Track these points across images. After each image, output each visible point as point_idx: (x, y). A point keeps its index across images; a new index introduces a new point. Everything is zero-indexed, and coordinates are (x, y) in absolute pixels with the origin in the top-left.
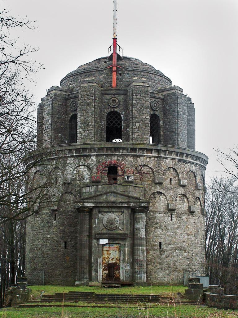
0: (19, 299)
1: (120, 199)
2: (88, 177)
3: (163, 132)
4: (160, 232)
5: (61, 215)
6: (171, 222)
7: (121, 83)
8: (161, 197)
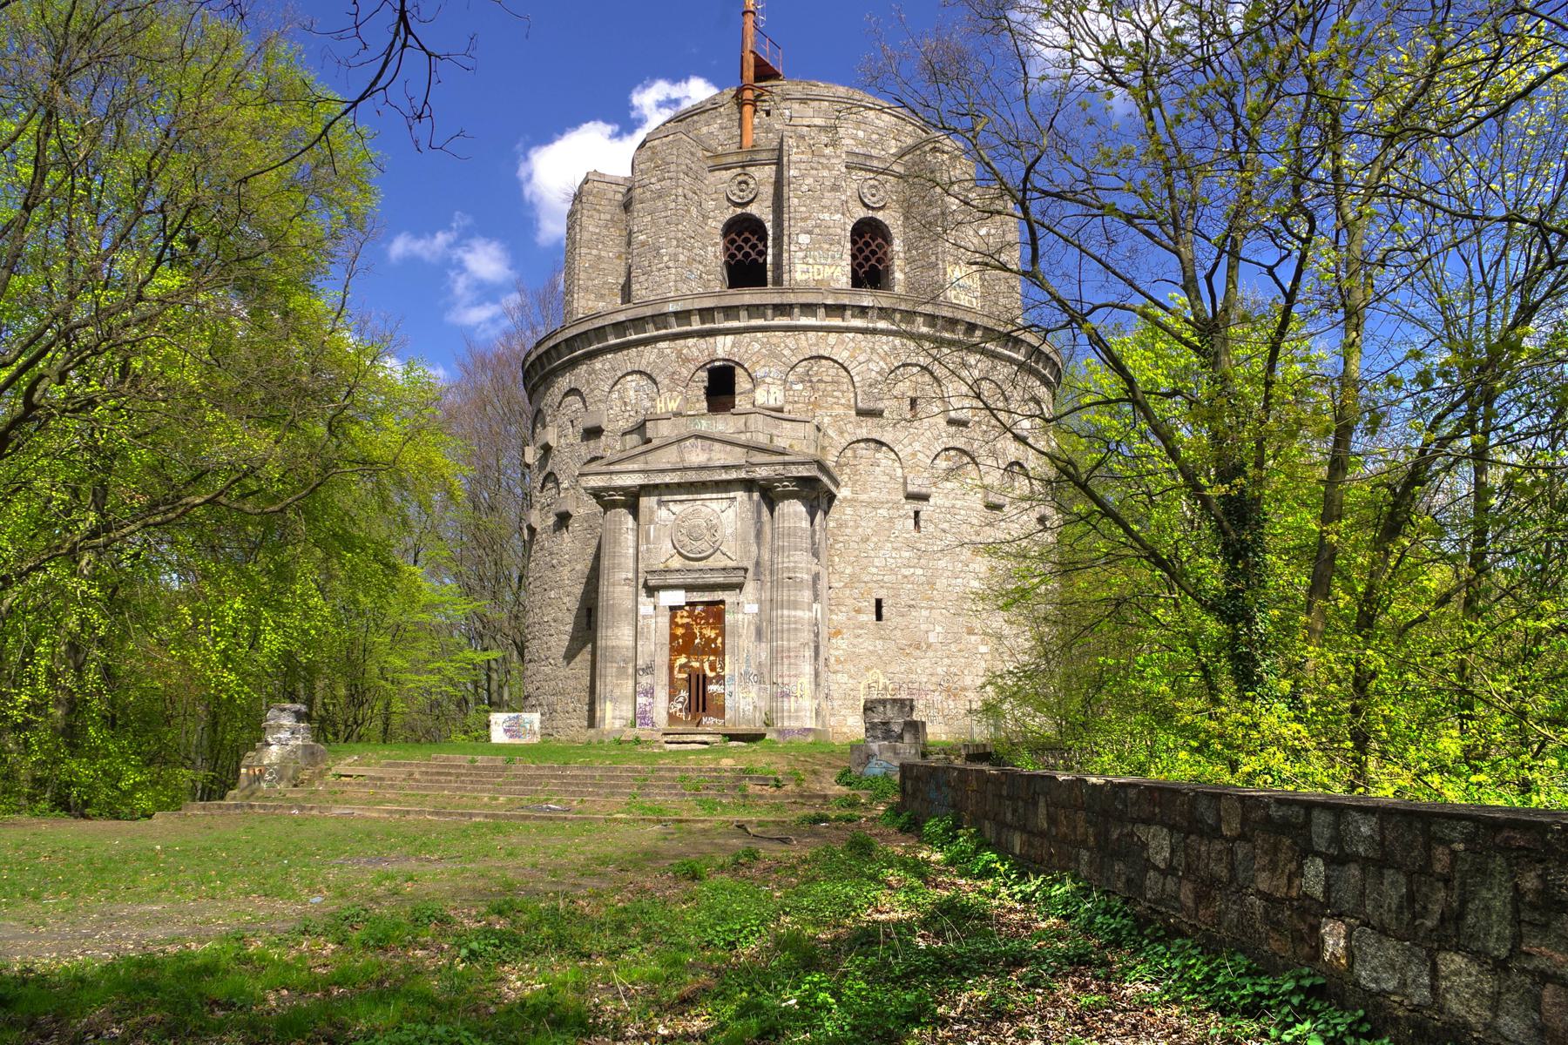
1: (721, 455)
7: (770, 135)
8: (877, 455)
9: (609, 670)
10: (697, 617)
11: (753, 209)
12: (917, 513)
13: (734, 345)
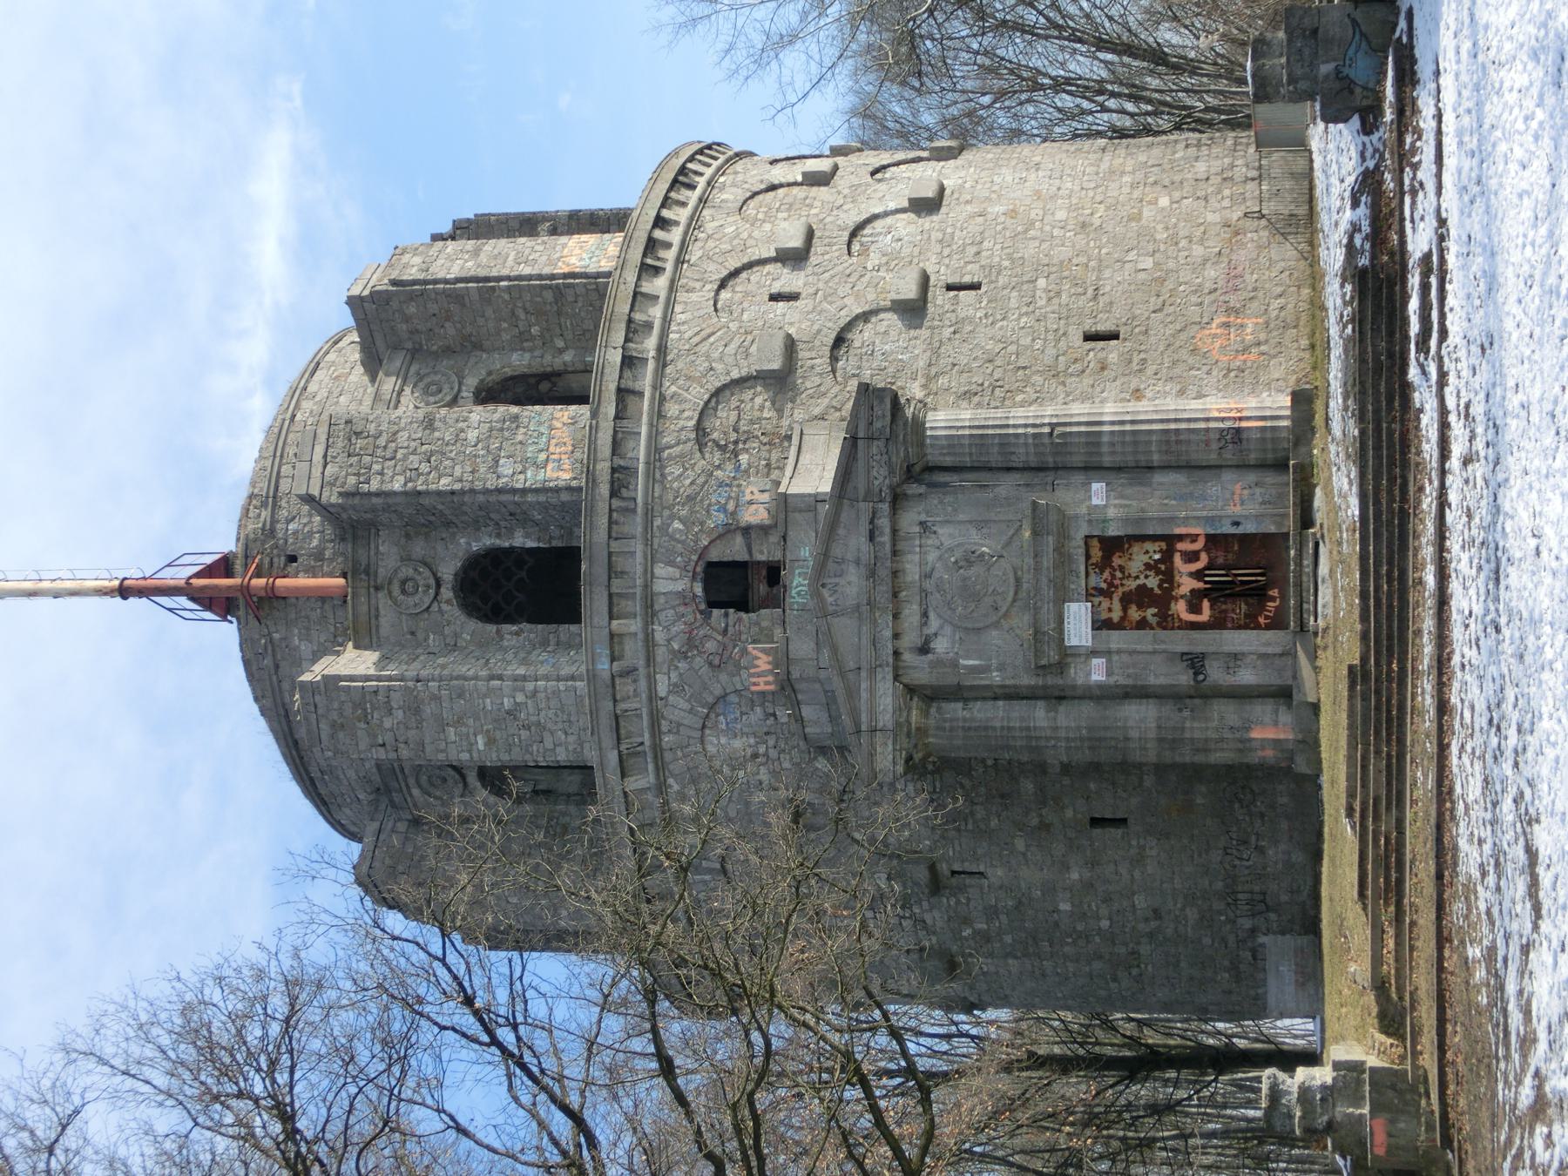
0: (1402, 1125)
2: (758, 710)
3: (561, 351)
4: (1033, 340)
5: (958, 848)
6: (984, 289)
8: (857, 344)
9: (1197, 735)
10: (1111, 585)
11: (448, 570)
12: (950, 288)
13: (671, 563)
